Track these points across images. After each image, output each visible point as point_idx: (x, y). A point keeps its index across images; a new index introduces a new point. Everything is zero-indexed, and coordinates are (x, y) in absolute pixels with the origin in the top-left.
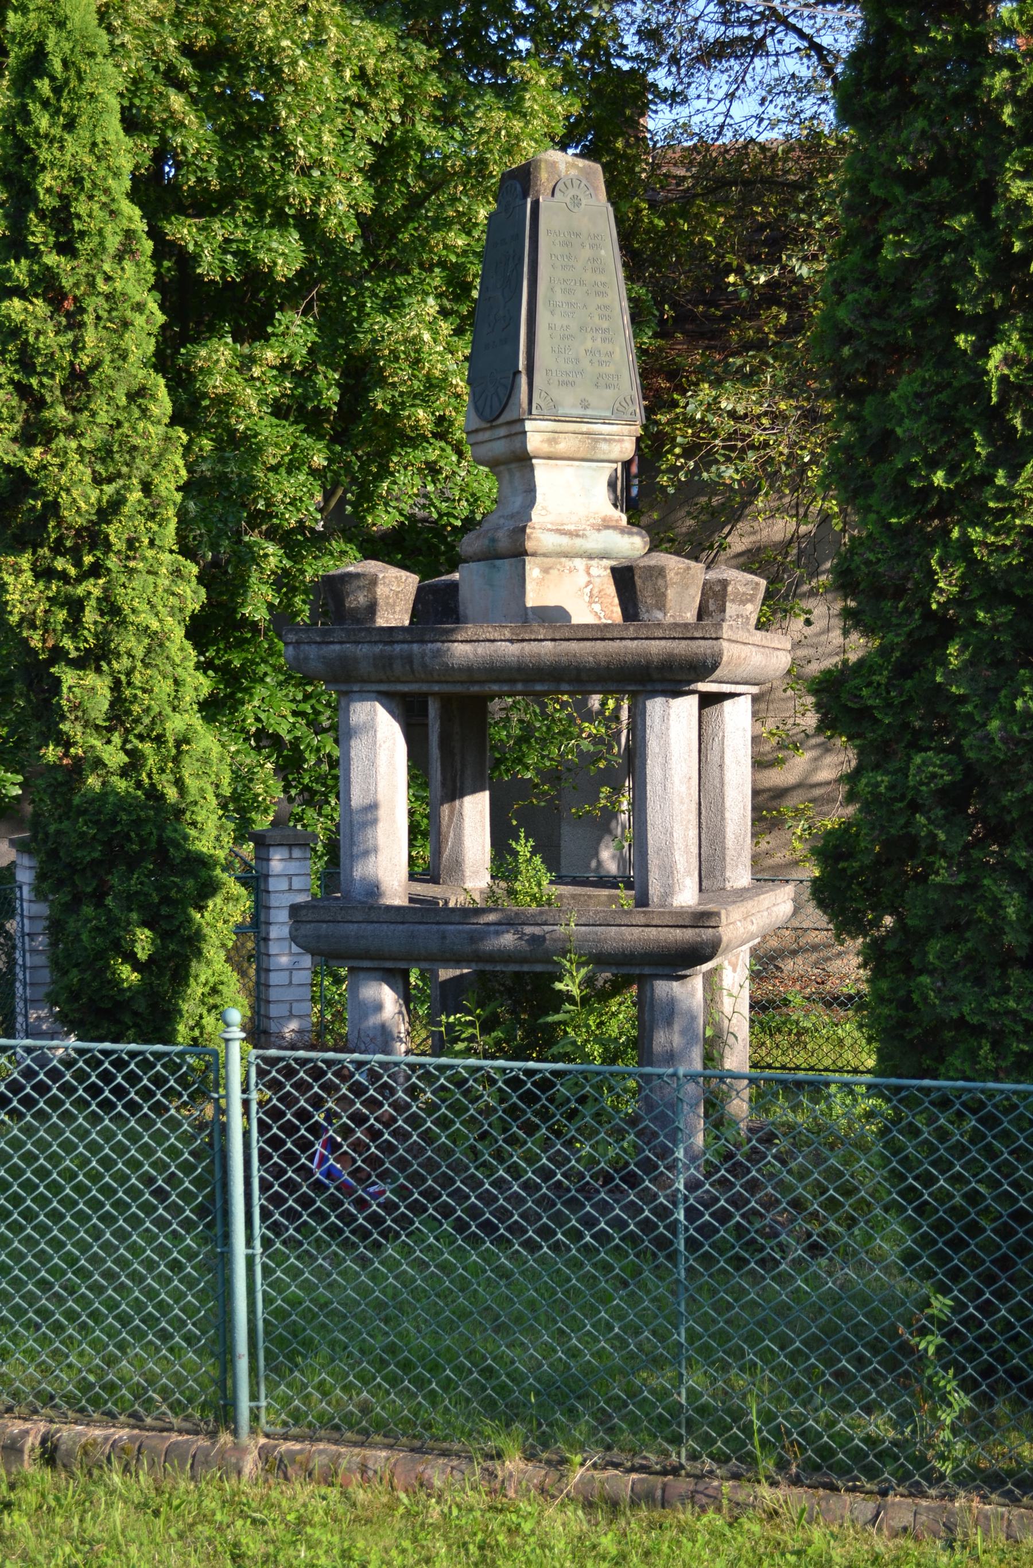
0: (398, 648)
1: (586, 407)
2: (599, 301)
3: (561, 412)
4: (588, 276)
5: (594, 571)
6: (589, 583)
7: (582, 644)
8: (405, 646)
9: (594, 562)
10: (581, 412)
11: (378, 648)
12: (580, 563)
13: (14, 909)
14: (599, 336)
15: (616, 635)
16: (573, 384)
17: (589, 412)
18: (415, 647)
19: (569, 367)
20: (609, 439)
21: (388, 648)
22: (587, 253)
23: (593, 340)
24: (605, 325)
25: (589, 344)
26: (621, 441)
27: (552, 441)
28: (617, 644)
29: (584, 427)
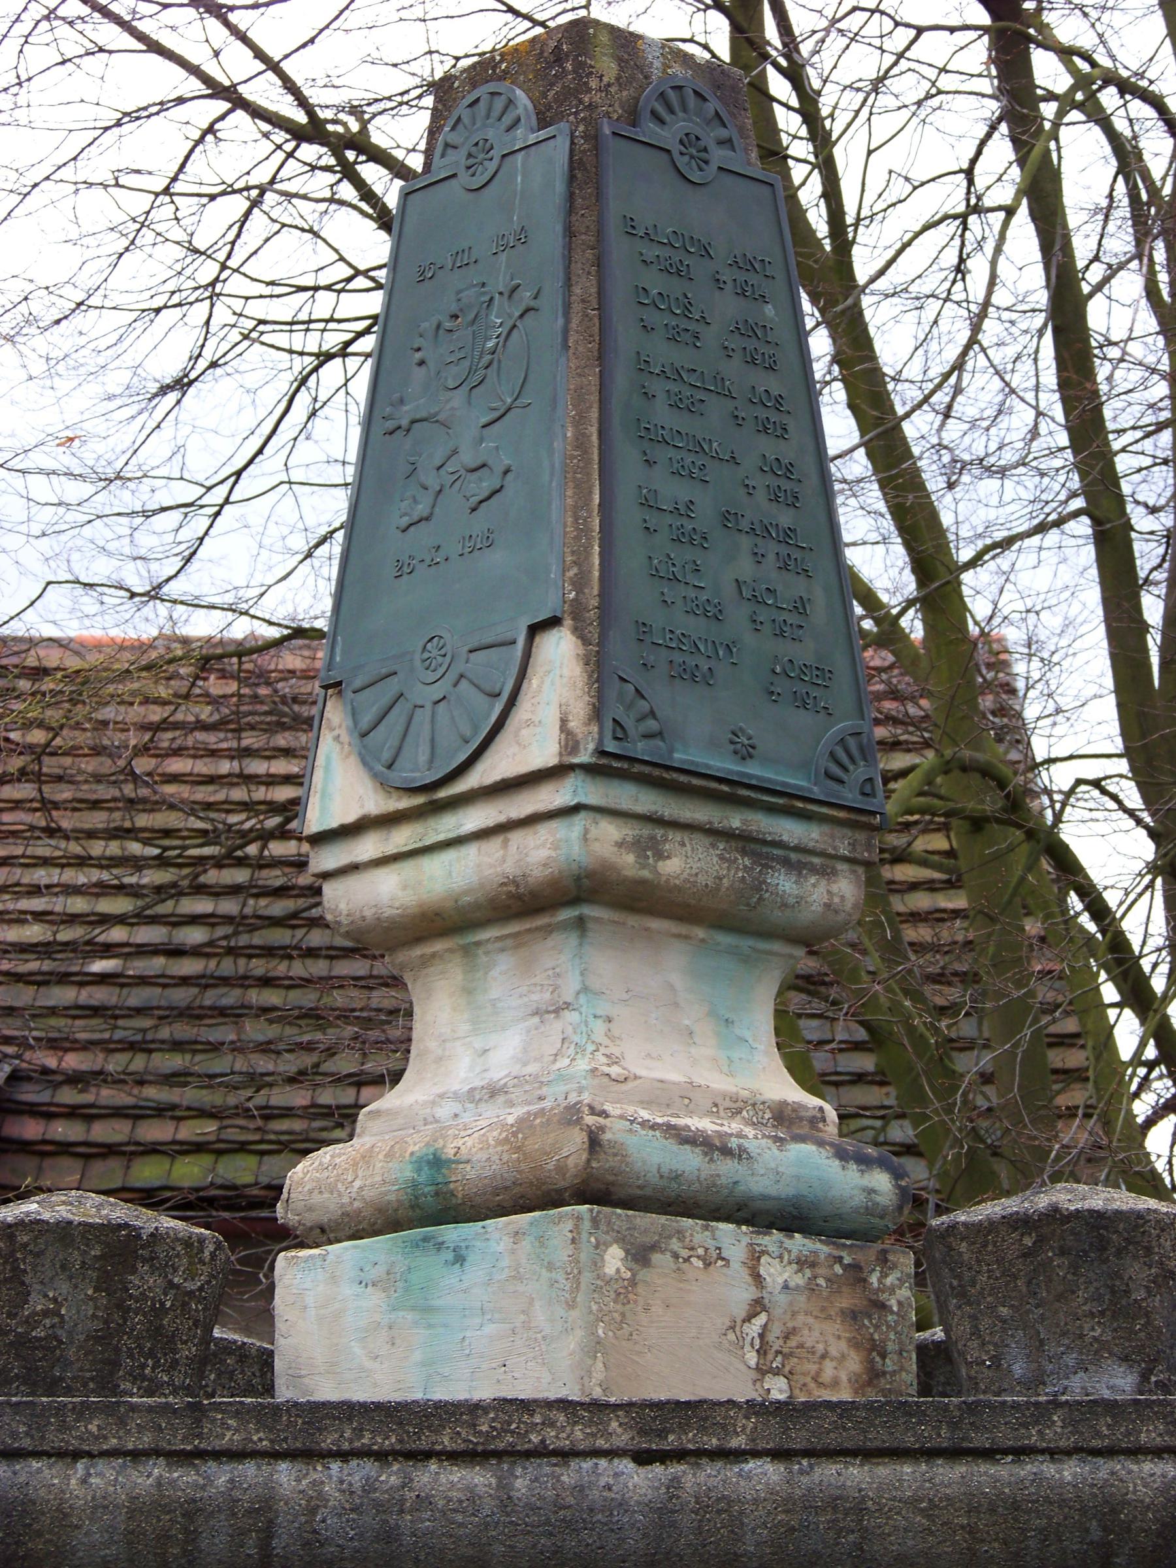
0: (221, 1475)
1: (746, 753)
2: (768, 447)
3: (679, 757)
4: (733, 369)
5: (776, 1273)
6: (758, 1306)
7: (884, 1471)
8: (249, 1470)
9: (772, 1240)
10: (723, 764)
11: (150, 1476)
12: (731, 1238)
13: (574, 23)
14: (771, 549)
15: (1003, 1437)
16: (707, 679)
17: (754, 770)
18: (285, 1475)
19: (695, 627)
20: (798, 860)
21: (185, 1477)
22: (726, 308)
23: (758, 558)
24: (785, 518)
25: (745, 568)
26: (827, 873)
27: (648, 849)
28: (1003, 1471)
29: (736, 820)
